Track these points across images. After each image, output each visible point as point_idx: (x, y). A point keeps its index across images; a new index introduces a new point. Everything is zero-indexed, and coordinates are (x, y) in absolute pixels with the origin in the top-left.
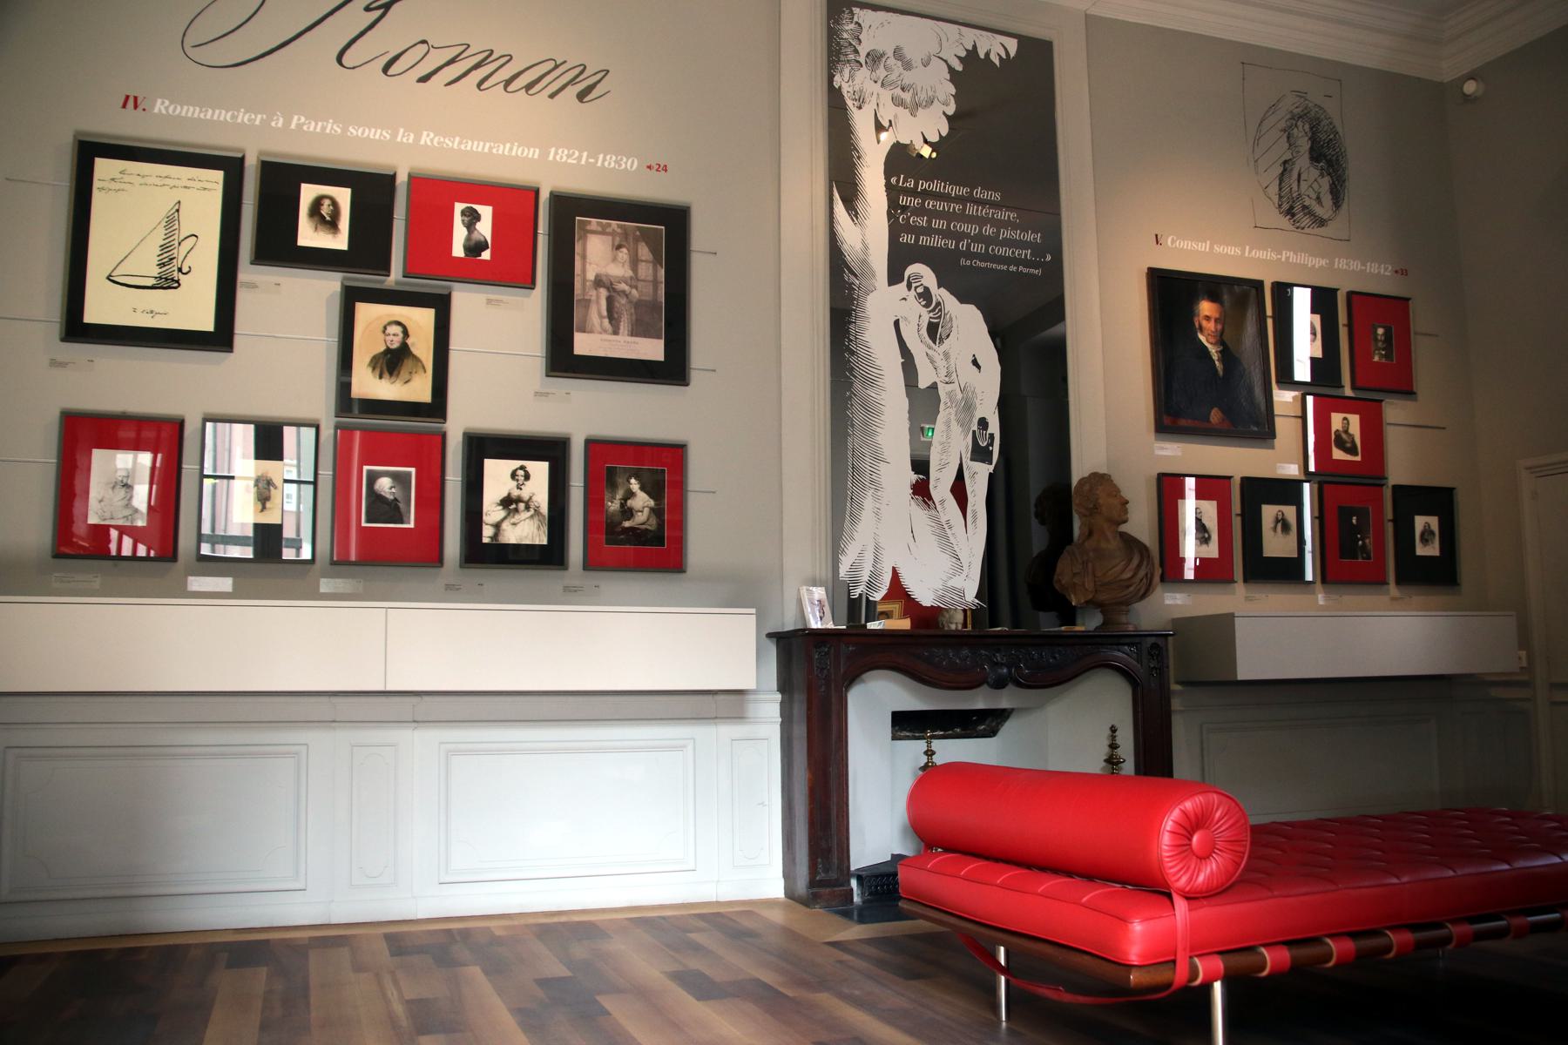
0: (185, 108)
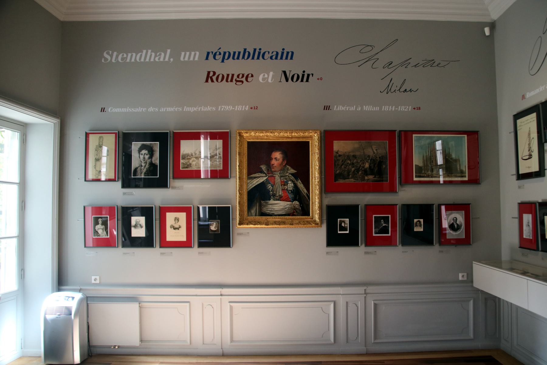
0: (117, 109)
